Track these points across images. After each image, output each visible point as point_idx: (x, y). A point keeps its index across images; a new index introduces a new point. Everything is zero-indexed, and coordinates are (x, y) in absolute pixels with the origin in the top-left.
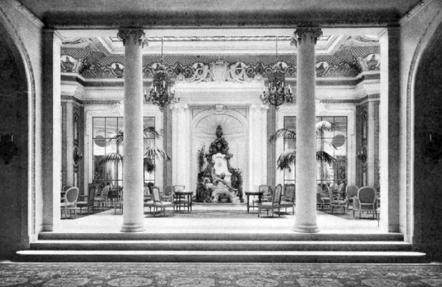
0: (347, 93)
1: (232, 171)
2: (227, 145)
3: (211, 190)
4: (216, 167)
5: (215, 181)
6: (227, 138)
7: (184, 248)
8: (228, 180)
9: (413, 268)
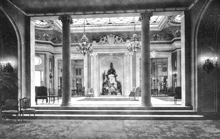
0: (167, 47)
1: (117, 82)
2: (115, 71)
3: (108, 90)
4: (110, 80)
5: (109, 86)
6: (115, 67)
7: (102, 113)
8: (116, 86)
9: (197, 123)
